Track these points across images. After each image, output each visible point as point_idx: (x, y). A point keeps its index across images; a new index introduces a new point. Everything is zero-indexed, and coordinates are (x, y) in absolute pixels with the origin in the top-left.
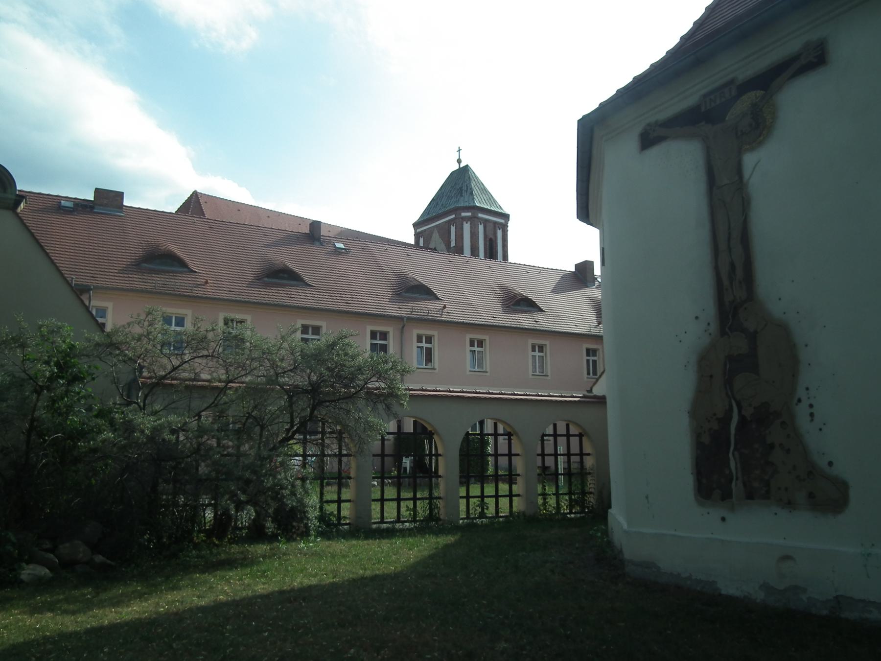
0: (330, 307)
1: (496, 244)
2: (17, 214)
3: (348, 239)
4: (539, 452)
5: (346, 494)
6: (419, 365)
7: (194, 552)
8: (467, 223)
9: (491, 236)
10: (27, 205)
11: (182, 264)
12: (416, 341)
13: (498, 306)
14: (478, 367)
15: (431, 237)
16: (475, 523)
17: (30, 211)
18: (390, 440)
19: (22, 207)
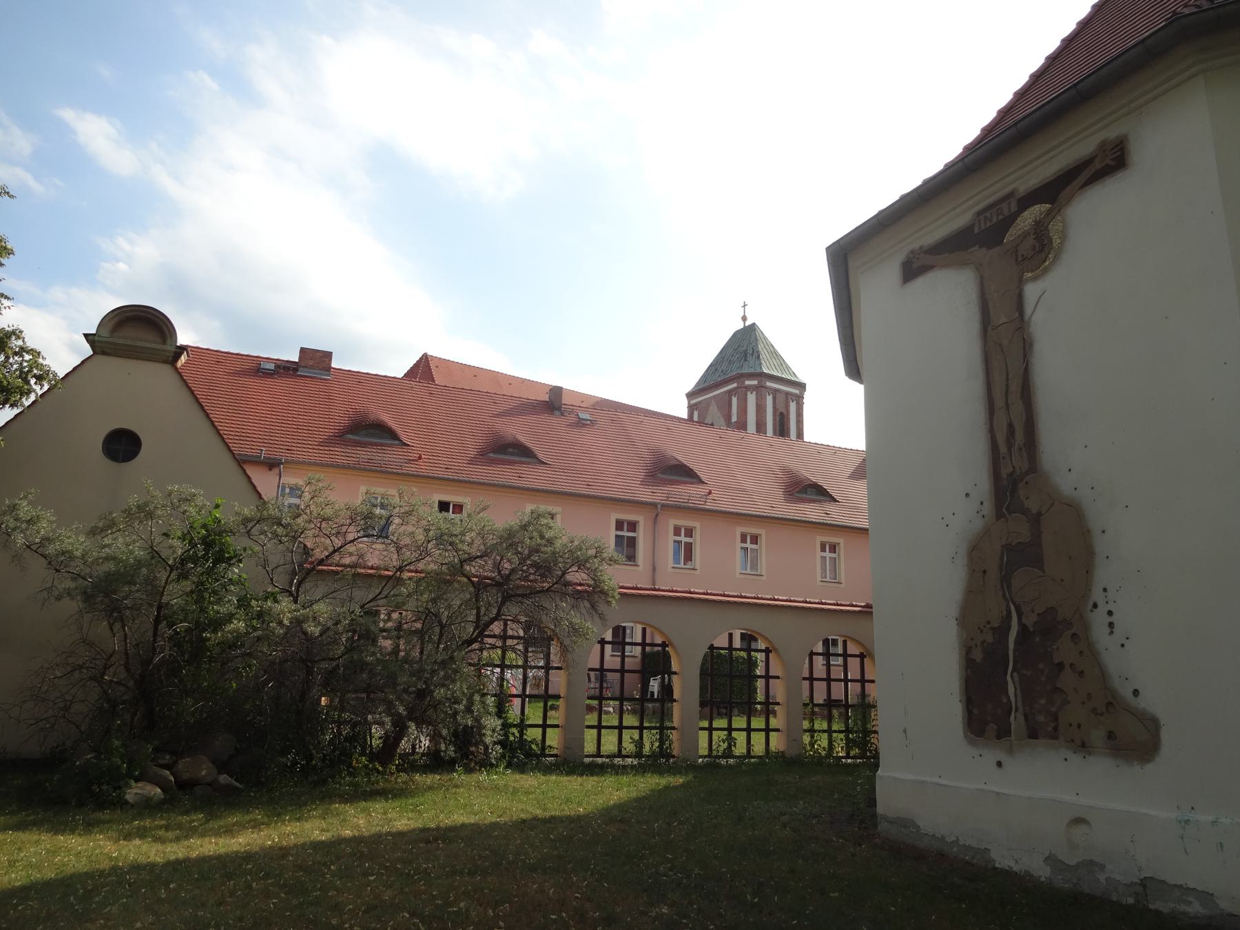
1: (788, 419)
2: (176, 369)
3: (595, 409)
5: (555, 717)
6: (677, 564)
9: (781, 409)
11: (393, 435)
12: (673, 534)
13: (779, 493)
14: (751, 569)
17: (225, 373)
18: (636, 657)
19: (184, 361)
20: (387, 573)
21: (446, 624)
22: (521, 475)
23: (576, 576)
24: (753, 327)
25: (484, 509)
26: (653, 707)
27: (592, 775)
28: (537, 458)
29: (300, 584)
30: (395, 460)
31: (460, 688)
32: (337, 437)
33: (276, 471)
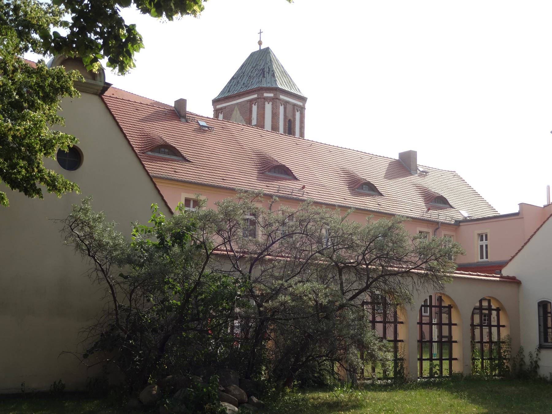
1: (294, 125)
2: (103, 100)
8: (268, 103)
9: (290, 117)
15: (231, 114)
22: (177, 171)
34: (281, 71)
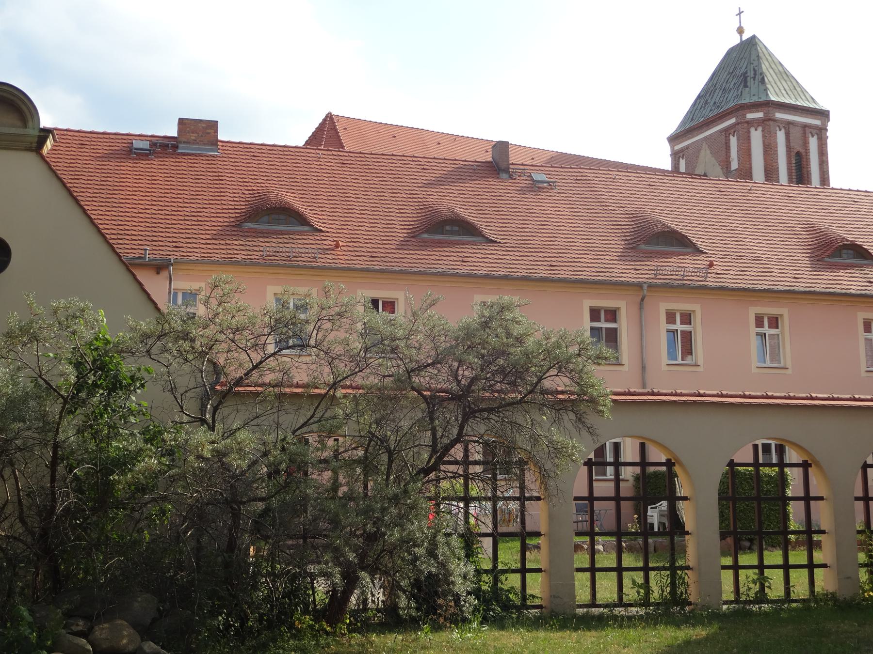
0: (525, 273)
2: (42, 157)
4: (860, 493)
7: (291, 642)
8: (756, 130)
9: (798, 147)
10: (56, 144)
11: (301, 220)
13: (804, 260)
14: (772, 361)
15: (697, 157)
16: (748, 610)
17: (91, 158)
19: (50, 147)
20: (317, 391)
21: (395, 449)
23: (556, 382)
24: (753, 42)
25: (432, 304)
26: (655, 542)
27: (590, 630)
28: (483, 236)
29: (215, 409)
30: (307, 251)
31: (419, 528)
32: (233, 226)
33: (165, 274)
34: (777, 71)
